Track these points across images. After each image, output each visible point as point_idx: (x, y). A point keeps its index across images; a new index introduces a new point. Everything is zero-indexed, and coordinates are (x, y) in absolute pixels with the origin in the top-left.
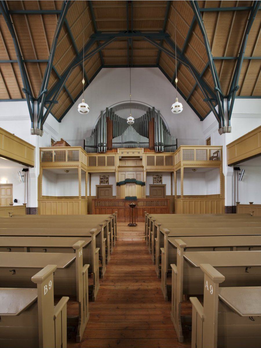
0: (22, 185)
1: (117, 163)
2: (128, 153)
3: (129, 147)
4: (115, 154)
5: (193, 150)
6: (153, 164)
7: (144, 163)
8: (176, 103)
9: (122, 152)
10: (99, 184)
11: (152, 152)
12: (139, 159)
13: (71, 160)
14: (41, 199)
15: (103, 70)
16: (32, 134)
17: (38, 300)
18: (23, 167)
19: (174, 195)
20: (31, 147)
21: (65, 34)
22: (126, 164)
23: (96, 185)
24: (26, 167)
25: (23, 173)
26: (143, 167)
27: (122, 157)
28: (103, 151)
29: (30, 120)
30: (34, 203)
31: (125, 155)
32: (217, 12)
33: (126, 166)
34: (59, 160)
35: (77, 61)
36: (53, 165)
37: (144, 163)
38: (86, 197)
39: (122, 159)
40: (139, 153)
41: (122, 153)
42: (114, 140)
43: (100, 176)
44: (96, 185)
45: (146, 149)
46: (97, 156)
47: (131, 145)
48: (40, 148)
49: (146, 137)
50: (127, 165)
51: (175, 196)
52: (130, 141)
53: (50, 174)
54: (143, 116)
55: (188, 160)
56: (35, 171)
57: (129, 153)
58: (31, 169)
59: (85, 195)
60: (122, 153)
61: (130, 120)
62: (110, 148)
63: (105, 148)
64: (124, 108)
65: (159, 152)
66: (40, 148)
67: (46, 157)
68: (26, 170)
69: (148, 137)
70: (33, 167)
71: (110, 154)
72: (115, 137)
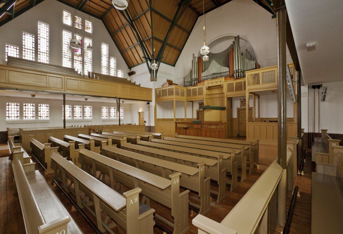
0: (148, 112)
1: (205, 91)
2: (212, 83)
3: (214, 78)
4: (203, 85)
5: (267, 73)
6: (232, 90)
7: (225, 89)
8: (204, 46)
9: (208, 83)
10: (240, 107)
11: (232, 79)
12: (220, 87)
13: (257, 83)
14: (157, 120)
15: (200, 18)
16: (151, 81)
17: (70, 147)
18: (147, 102)
19: (292, 116)
20: (150, 90)
21: (75, 68)
22: (213, 92)
23: (237, 108)
24: (148, 102)
25: (147, 105)
26: (224, 93)
27: (209, 87)
28: (239, 76)
29: (149, 73)
30: (153, 124)
31: (210, 85)
32: (144, 14)
33: (213, 93)
34: (253, 83)
35: (173, 23)
36: (163, 98)
37: (225, 89)
38: (185, 119)
39: (209, 88)
40: (221, 82)
41: (208, 84)
42: (203, 74)
43: (241, 99)
44: (237, 108)
45: (226, 77)
46: (191, 88)
47: (215, 76)
48: (155, 89)
49: (228, 67)
50: (214, 93)
51: (185, 119)
52: (214, 73)
53: (167, 105)
54: (230, 46)
55: (270, 82)
56: (153, 104)
57: (213, 83)
58: (150, 103)
59: (191, 118)
60: (208, 84)
61: (204, 58)
62: (199, 81)
63: (240, 73)
64: (219, 43)
65: (238, 78)
66: (155, 89)
67: (158, 96)
68: (148, 103)
69: (229, 67)
70: (151, 101)
71: (199, 86)
72: (204, 71)
